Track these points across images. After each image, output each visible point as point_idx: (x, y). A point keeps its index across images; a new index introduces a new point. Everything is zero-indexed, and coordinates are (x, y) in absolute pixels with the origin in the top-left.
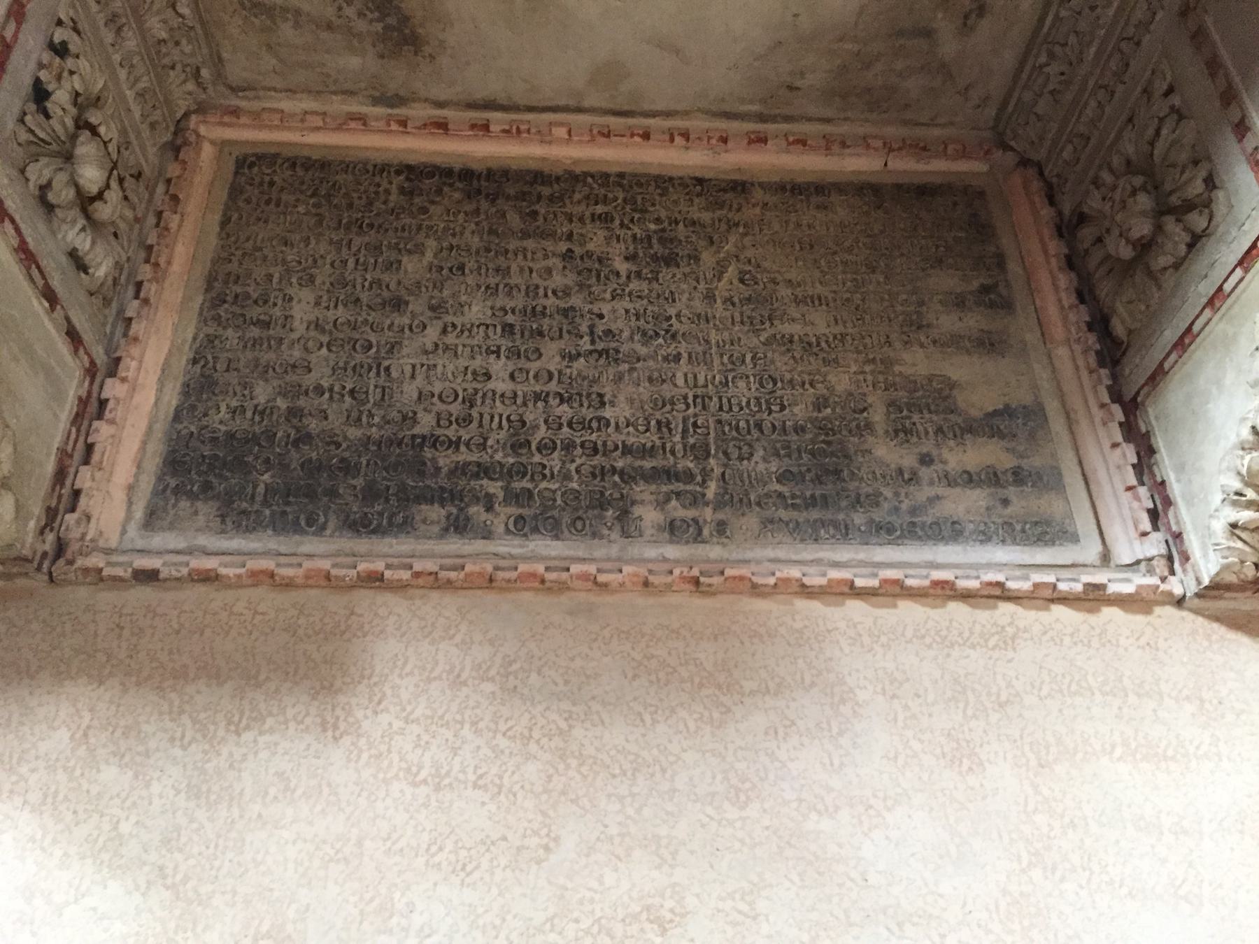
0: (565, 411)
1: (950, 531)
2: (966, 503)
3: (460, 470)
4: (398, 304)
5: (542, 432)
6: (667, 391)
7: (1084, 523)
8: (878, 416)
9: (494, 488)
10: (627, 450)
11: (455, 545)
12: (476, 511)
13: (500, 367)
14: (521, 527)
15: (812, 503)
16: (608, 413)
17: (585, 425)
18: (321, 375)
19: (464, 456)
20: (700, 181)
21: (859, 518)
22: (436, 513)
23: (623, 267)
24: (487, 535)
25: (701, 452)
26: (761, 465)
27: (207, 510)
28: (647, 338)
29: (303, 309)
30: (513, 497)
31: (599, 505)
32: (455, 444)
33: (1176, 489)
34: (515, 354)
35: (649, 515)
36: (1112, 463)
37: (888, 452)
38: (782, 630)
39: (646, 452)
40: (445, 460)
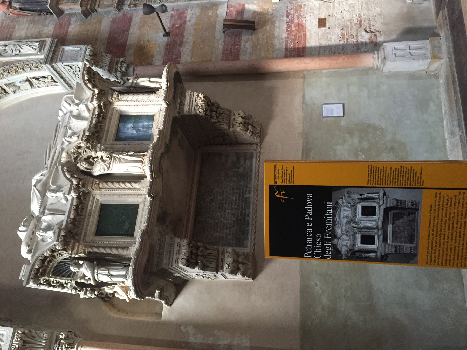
0: (234, 204)
1: (251, 165)
2: (248, 163)
3: (241, 215)
4: (217, 223)
5: (236, 207)
6: (231, 193)
7: (251, 151)
8: (237, 170)
9: (243, 212)
10: (239, 197)
11: (251, 216)
12: (247, 213)
13: (227, 211)
14: (249, 208)
15: (247, 178)
16: (234, 199)
17: (236, 202)
18: (228, 231)
19: (239, 215)
20: (198, 187)
21: (249, 174)
22: (247, 218)
23: (212, 197)
24: (249, 212)
25: (240, 189)
26: (242, 183)
27: (245, 242)
28: (223, 195)
29: (218, 234)
30: (245, 209)
31: (246, 201)
32: (238, 216)
33: (249, 142)
34: (225, 209)
35: (248, 196)
36: (244, 147)
37: (241, 170)
38: (46, 71)
39: (240, 196)
40: (240, 217)
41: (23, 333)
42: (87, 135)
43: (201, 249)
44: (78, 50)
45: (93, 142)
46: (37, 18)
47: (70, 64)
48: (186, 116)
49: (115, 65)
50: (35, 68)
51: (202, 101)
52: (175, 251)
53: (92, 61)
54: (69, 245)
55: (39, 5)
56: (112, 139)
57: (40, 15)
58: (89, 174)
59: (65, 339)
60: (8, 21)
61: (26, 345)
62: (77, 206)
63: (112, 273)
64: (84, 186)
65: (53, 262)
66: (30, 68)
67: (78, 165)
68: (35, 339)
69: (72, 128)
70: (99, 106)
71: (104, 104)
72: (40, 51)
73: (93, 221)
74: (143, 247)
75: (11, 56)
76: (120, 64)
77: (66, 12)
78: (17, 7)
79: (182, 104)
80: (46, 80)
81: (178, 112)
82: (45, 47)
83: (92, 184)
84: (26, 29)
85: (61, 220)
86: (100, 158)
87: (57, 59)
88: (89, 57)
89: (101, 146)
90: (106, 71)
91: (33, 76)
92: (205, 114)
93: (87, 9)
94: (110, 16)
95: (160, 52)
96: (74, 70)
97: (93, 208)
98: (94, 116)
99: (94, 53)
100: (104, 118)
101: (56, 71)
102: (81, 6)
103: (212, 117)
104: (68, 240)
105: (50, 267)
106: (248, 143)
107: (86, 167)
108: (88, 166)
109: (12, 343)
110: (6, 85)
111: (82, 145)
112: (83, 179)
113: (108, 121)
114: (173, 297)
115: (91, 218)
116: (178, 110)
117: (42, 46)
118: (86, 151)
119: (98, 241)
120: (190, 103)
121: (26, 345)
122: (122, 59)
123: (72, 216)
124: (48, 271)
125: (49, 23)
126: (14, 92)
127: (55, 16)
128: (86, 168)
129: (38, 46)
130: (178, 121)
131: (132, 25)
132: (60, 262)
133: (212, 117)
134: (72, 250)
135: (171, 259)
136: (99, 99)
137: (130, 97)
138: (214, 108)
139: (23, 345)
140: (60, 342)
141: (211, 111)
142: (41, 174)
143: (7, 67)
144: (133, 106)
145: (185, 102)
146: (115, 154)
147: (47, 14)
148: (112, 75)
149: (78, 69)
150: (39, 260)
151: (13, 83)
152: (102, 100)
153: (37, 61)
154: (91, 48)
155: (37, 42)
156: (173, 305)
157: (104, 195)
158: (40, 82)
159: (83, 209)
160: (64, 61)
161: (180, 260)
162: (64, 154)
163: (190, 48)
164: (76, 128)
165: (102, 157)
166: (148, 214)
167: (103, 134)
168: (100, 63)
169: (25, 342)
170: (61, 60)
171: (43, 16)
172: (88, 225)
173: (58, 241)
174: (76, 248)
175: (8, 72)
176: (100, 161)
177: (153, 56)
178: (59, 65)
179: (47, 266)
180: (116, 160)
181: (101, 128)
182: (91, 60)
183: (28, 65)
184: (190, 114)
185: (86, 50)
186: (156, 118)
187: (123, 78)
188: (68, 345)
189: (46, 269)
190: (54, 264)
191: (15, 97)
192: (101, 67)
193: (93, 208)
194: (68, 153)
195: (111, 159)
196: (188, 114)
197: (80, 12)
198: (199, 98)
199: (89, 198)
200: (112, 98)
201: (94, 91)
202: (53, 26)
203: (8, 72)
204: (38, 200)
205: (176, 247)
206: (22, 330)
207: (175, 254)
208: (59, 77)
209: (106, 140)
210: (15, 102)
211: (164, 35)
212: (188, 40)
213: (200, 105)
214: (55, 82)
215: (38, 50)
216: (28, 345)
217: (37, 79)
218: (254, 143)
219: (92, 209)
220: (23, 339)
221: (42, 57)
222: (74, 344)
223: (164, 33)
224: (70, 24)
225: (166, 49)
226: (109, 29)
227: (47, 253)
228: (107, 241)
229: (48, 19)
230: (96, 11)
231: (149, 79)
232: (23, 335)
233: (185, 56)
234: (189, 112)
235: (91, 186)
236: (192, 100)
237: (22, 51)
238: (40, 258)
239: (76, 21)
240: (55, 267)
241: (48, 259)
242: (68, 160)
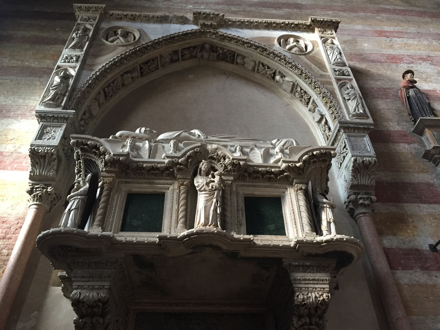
41: (52, 154)
42: (239, 163)
43: (101, 320)
44: (367, 149)
45: (234, 171)
46: (406, 114)
47: (347, 146)
48: (288, 277)
49: (364, 191)
50: (333, 116)
51: (316, 297)
52: (92, 283)
53: (357, 165)
54: (111, 167)
55: (420, 111)
56: (245, 192)
57: (410, 115)
58: (195, 175)
59: (47, 192)
60: (393, 93)
61: (41, 158)
62: (158, 169)
63: (72, 213)
64: (179, 170)
65: (95, 157)
66: (333, 113)
67: (203, 161)
69: (253, 151)
70: (282, 172)
71: (286, 175)
72: (354, 116)
73: (143, 188)
74: (91, 240)
75: (342, 95)
76: (367, 196)
77: (423, 138)
78: (410, 93)
79: (305, 269)
80: (327, 131)
81: (290, 265)
82: (360, 119)
83: (183, 179)
84: (388, 108)
85: (143, 156)
86: (212, 179)
87: (349, 132)
88: (361, 161)
89: (231, 180)
90: (351, 183)
91: (328, 120)
92: (299, 306)
93: (433, 155)
94: (435, 180)
95: (405, 243)
96: (343, 152)
97: (159, 185)
98: (268, 169)
99: (369, 165)
100: (270, 179)
101: (337, 135)
102: (434, 148)
103: (300, 317)
104: (117, 165)
105: (91, 155)
107: (203, 169)
108: (204, 171)
109: (43, 147)
110: (314, 101)
111: (227, 160)
112: (187, 167)
113: (268, 184)
115: (146, 185)
116: (293, 263)
117: (359, 116)
118: (222, 166)
119: (118, 196)
120: (309, 280)
121: (41, 158)
122: (374, 198)
124: (87, 154)
125: (403, 125)
126: (310, 110)
127: (413, 129)
128: (201, 169)
129: (359, 112)
130: (281, 266)
131: (432, 205)
132: (96, 163)
133: (300, 317)
134: (106, 171)
135: (83, 279)
136: (288, 168)
137: (302, 203)
138: (314, 320)
139: (42, 156)
140: (45, 188)
141: (310, 316)
142: (200, 134)
143: (329, 94)
144: (291, 208)
145: (310, 272)
146: (217, 193)
147: (413, 121)
148: (349, 191)
149: (345, 155)
150: (97, 143)
151: (317, 106)
152: (290, 173)
153: (341, 116)
154: (373, 162)
155: (364, 111)
156: (65, 298)
157: (173, 195)
158: (324, 127)
159: (155, 175)
160: (349, 139)
161: (79, 291)
162: (214, 146)
163: (422, 281)
164: (253, 154)
165: (214, 181)
166: (138, 242)
167: (249, 182)
168: (359, 175)
169: (45, 157)
170: (349, 137)
171: (409, 118)
172: (138, 183)
173: (114, 155)
174: (110, 175)
175: (323, 97)
176: (208, 180)
177: (395, 235)
178: (343, 136)
179: (91, 153)
180: (209, 196)
181: (256, 178)
182: (358, 164)
183: (336, 109)
184: (293, 282)
185: (370, 157)
186: (280, 238)
187: (351, 204)
188: (40, 195)
189: (88, 152)
190: (93, 158)
191: (306, 113)
192: (354, 176)
193: (158, 186)
194: (217, 149)
195: (211, 190)
196: (292, 278)
197: (428, 148)
198: (320, 293)
200: (296, 183)
201: (298, 162)
202: (400, 129)
203: (323, 97)
204: (170, 135)
205: (97, 284)
206: (55, 153)
207: (88, 283)
208: (332, 141)
209: (242, 186)
210: (301, 115)
211: (430, 246)
212: (434, 278)
213: (310, 295)
214: (328, 139)
215: (354, 113)
216: (42, 160)
217: (326, 123)
219: (157, 184)
220: (47, 155)
221: (348, 119)
223: (434, 244)
224: (409, 143)
225: (411, 250)
226: (416, 181)
227: (102, 148)
228: (116, 204)
229: (407, 123)
230: (437, 166)
231: (331, 221)
233: (408, 275)
234: (295, 280)
235: (180, 177)
236: (314, 282)
237: (350, 101)
238: (98, 144)
239: (415, 149)
240: (92, 160)
241: (97, 151)
242: (210, 151)
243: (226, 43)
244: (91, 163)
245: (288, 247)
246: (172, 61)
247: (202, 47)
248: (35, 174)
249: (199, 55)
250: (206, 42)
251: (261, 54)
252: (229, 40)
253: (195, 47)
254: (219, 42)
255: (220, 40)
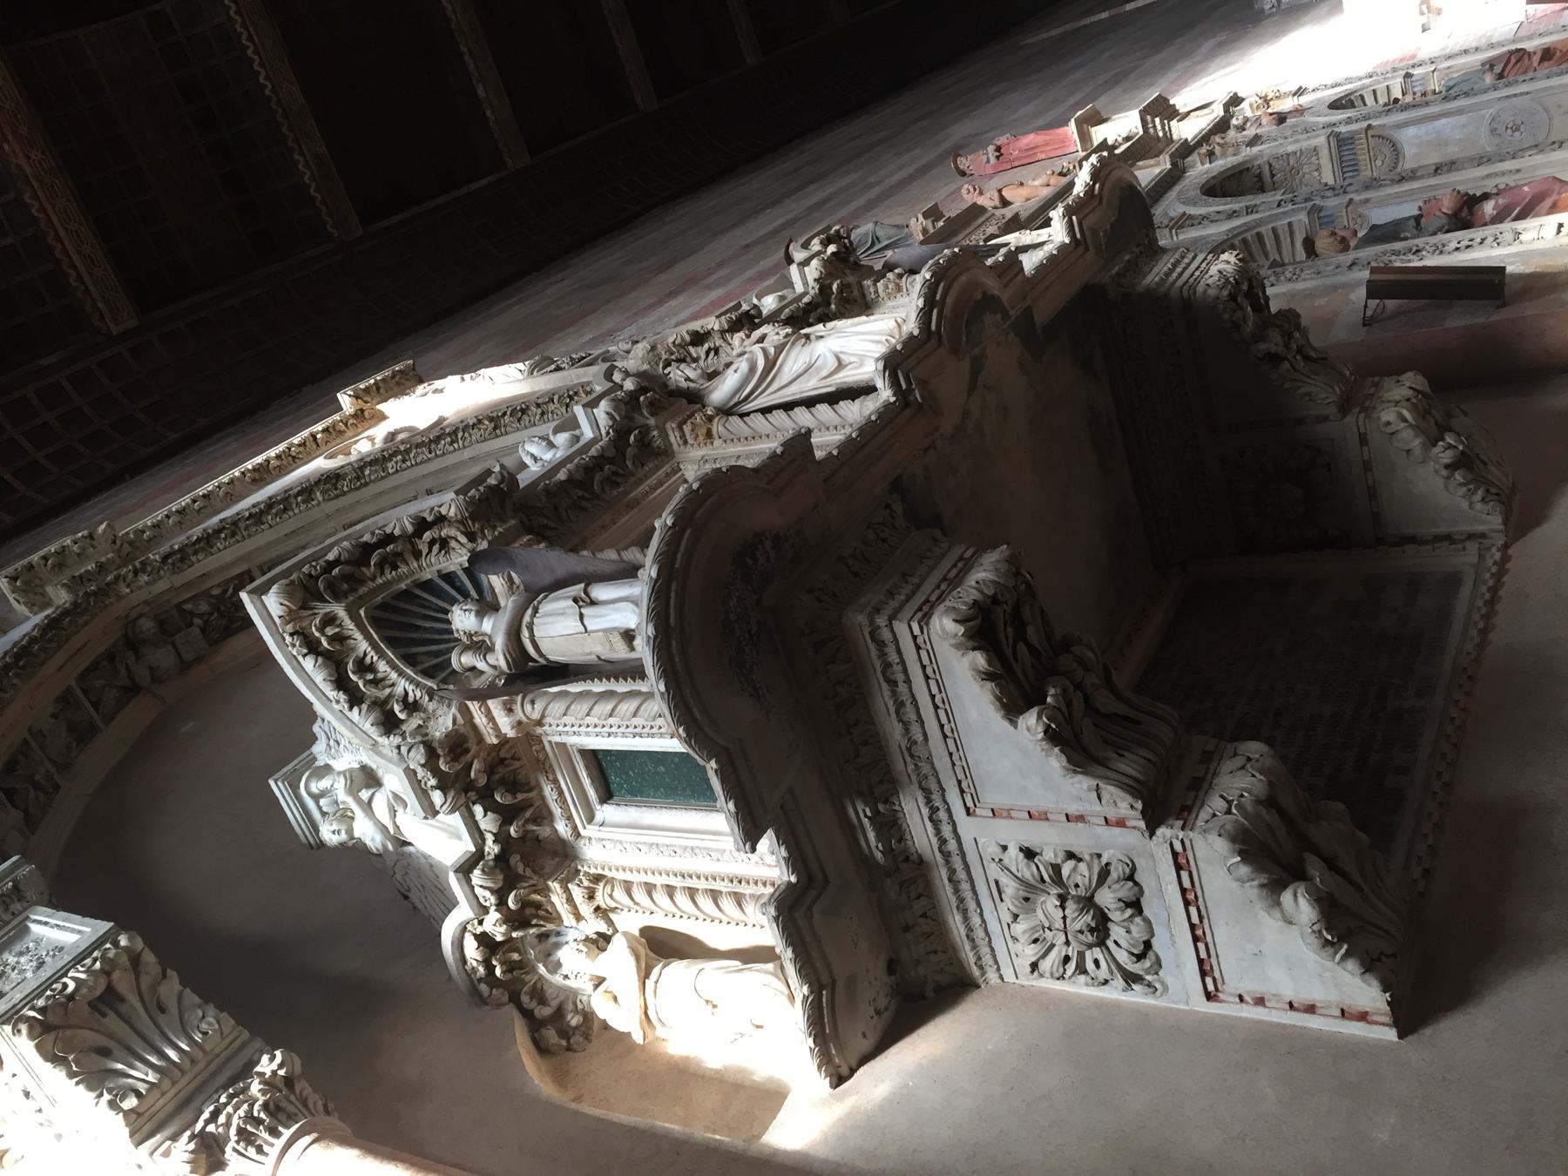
68: (161, 1019)
106: (1438, 538)
114: (866, 1045)
123: (562, 476)
124: (362, 590)
159: (611, 482)
190: (400, 579)
199: (658, 468)
206: (139, 944)
216: (112, 1021)
218: (1471, 536)
222: (290, 1119)
232: (124, 960)
242: (646, 367)
243: (203, 565)
244: (405, 612)
245: (1062, 248)
246: (83, 734)
247: (132, 643)
248: (142, 1088)
249: (142, 675)
250: (133, 615)
251: (337, 497)
252: (203, 549)
253: (110, 656)
254: (179, 580)
255: (176, 570)
